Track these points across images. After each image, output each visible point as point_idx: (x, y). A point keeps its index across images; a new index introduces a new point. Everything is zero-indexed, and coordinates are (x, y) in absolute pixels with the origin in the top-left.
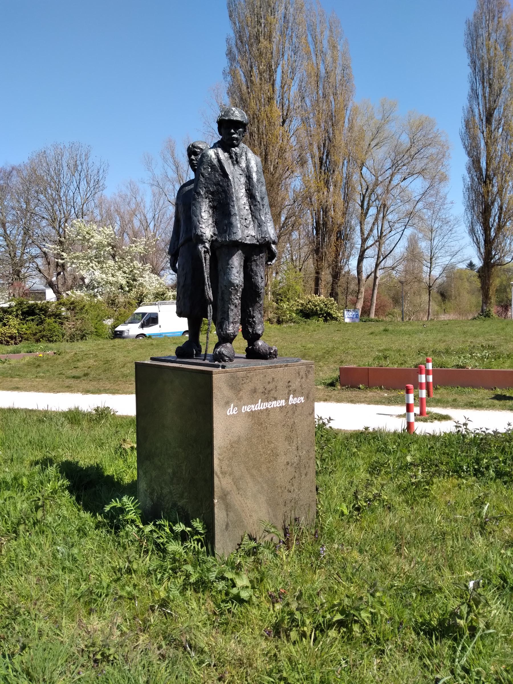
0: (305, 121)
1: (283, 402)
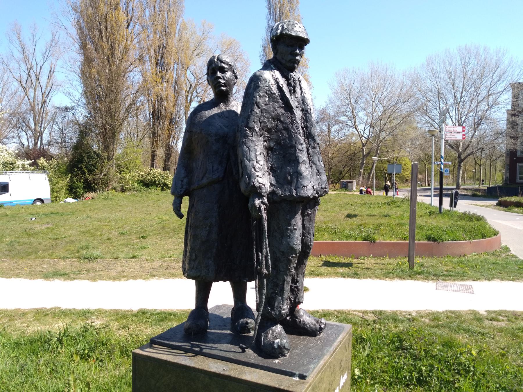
0: (144, 28)
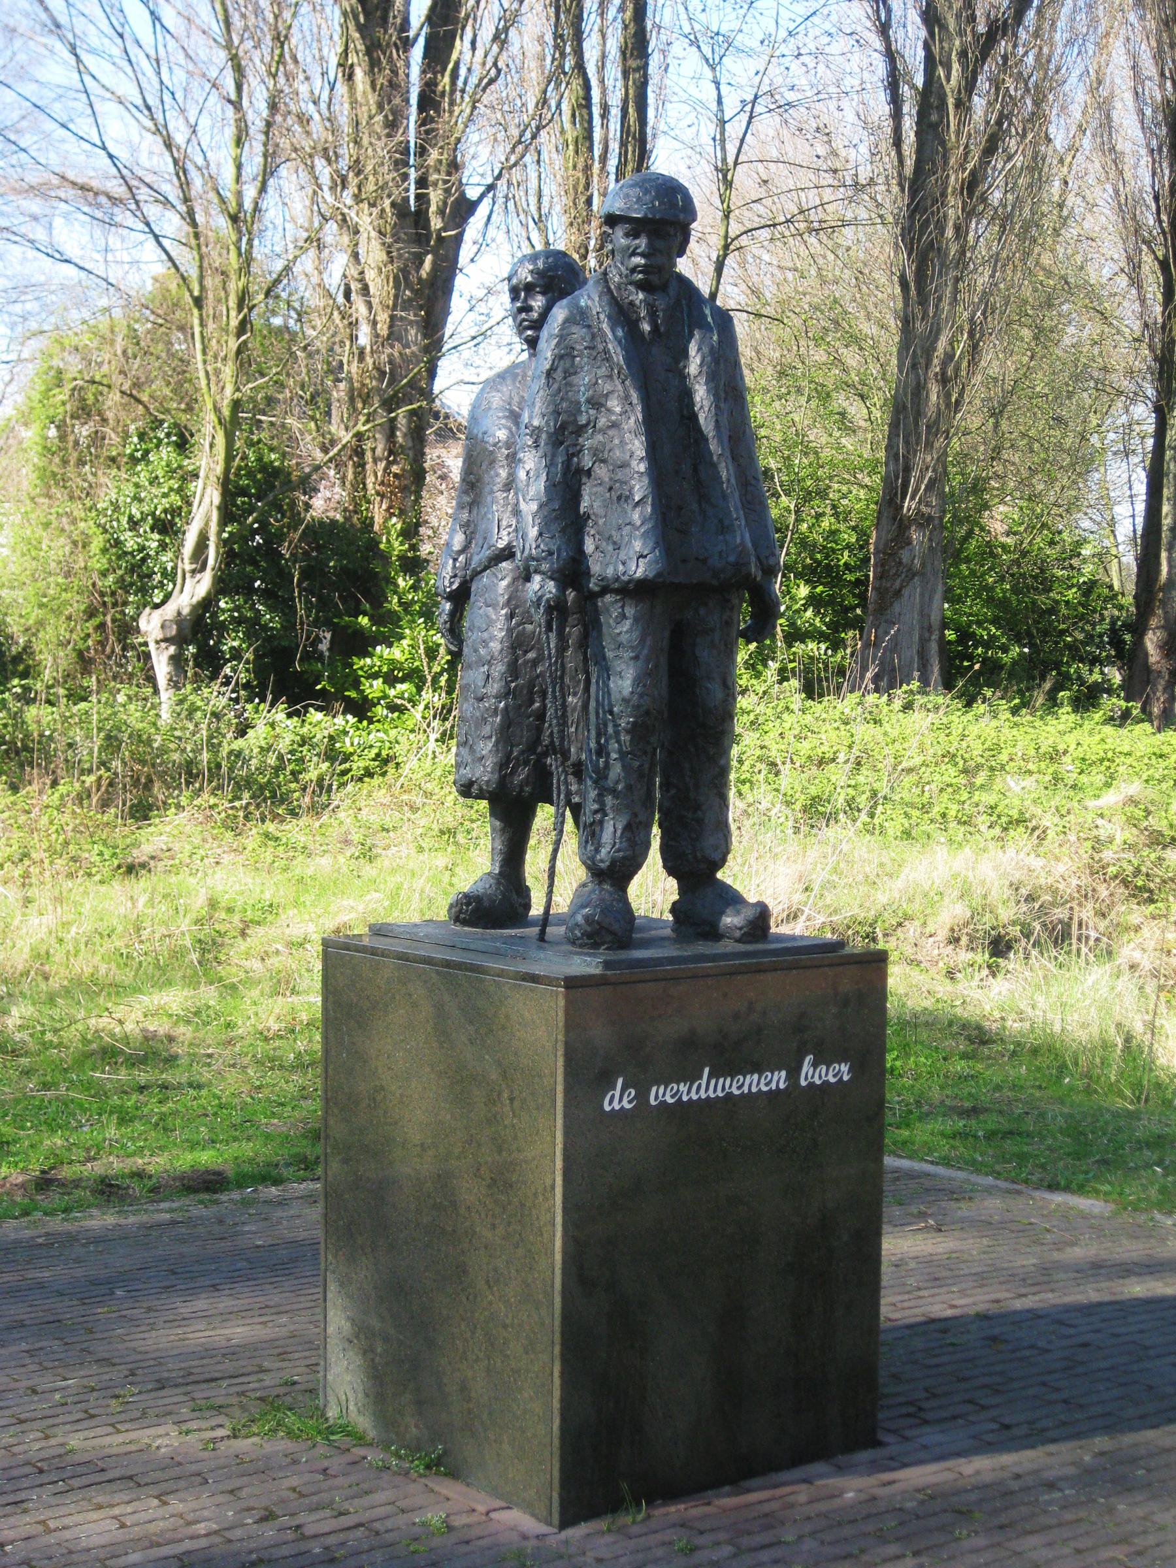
1: (778, 1079)
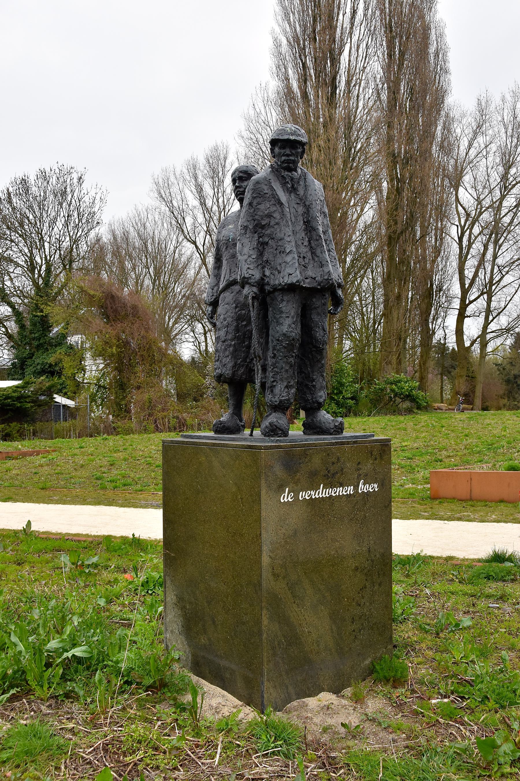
1: (350, 490)
